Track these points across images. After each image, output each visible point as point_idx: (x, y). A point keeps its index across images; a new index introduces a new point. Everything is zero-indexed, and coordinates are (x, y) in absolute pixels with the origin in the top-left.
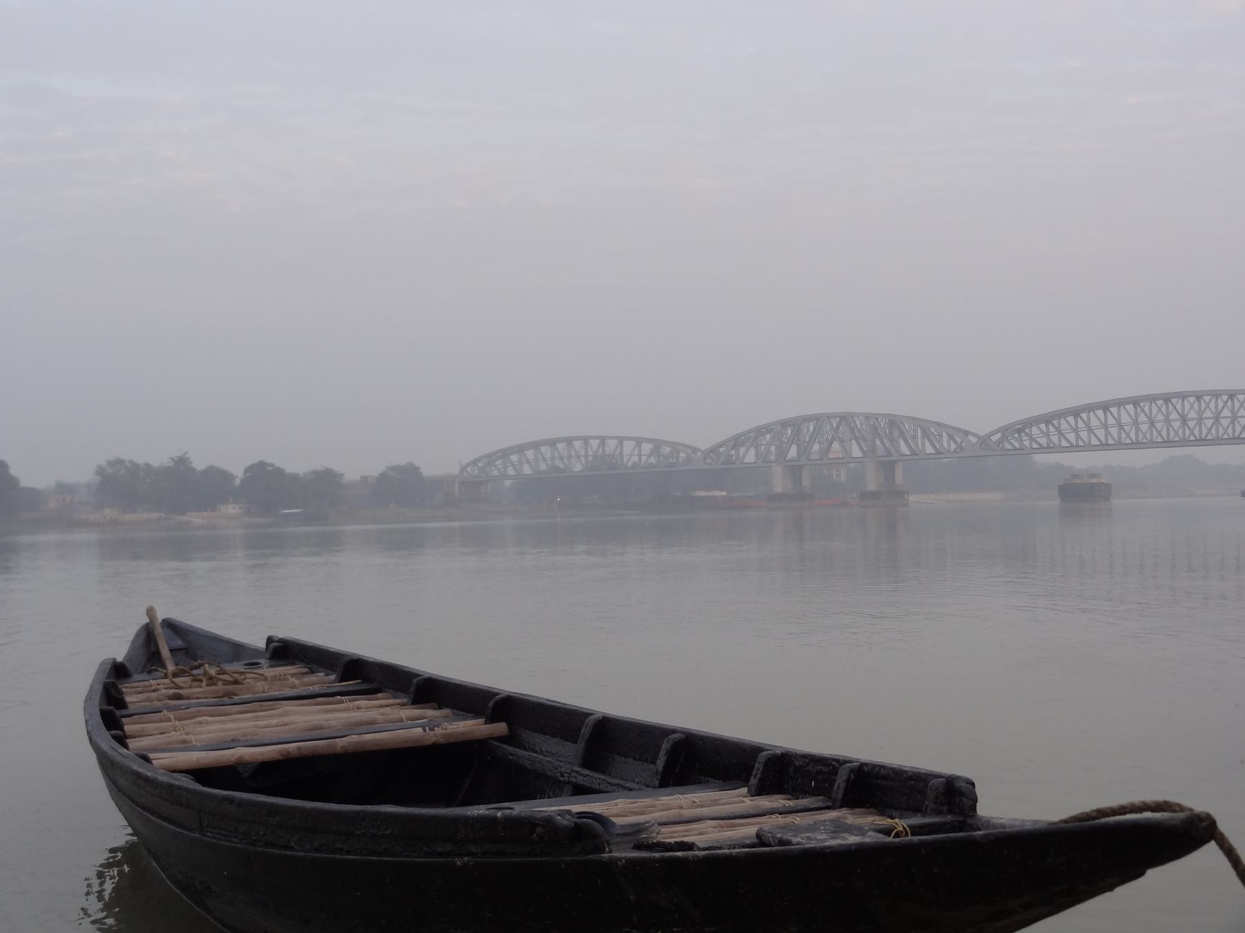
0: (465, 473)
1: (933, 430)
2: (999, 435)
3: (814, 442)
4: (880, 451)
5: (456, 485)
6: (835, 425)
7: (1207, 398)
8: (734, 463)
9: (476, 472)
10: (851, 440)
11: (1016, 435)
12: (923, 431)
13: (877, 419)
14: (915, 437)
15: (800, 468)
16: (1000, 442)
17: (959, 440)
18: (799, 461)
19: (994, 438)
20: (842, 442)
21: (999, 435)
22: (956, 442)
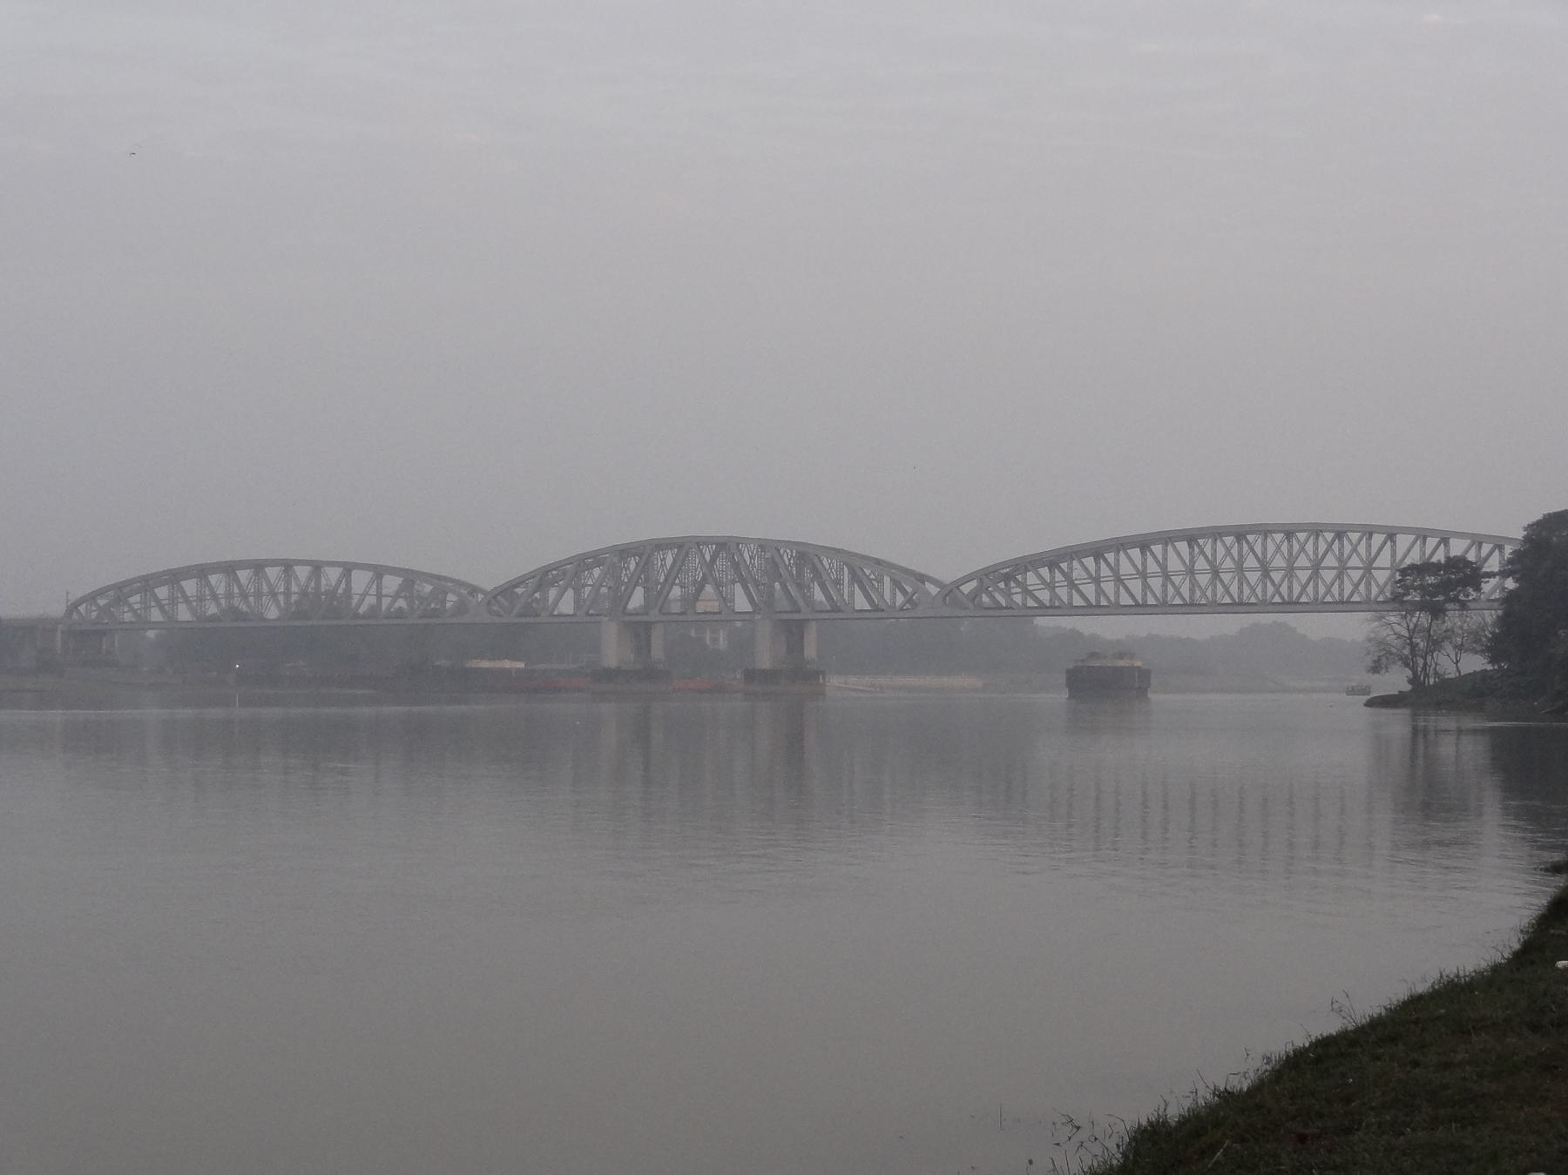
0: (75, 616)
2: (974, 584)
3: (673, 584)
4: (783, 604)
6: (708, 558)
9: (94, 614)
11: (1002, 585)
14: (838, 582)
15: (648, 626)
16: (975, 595)
17: (909, 589)
21: (974, 584)
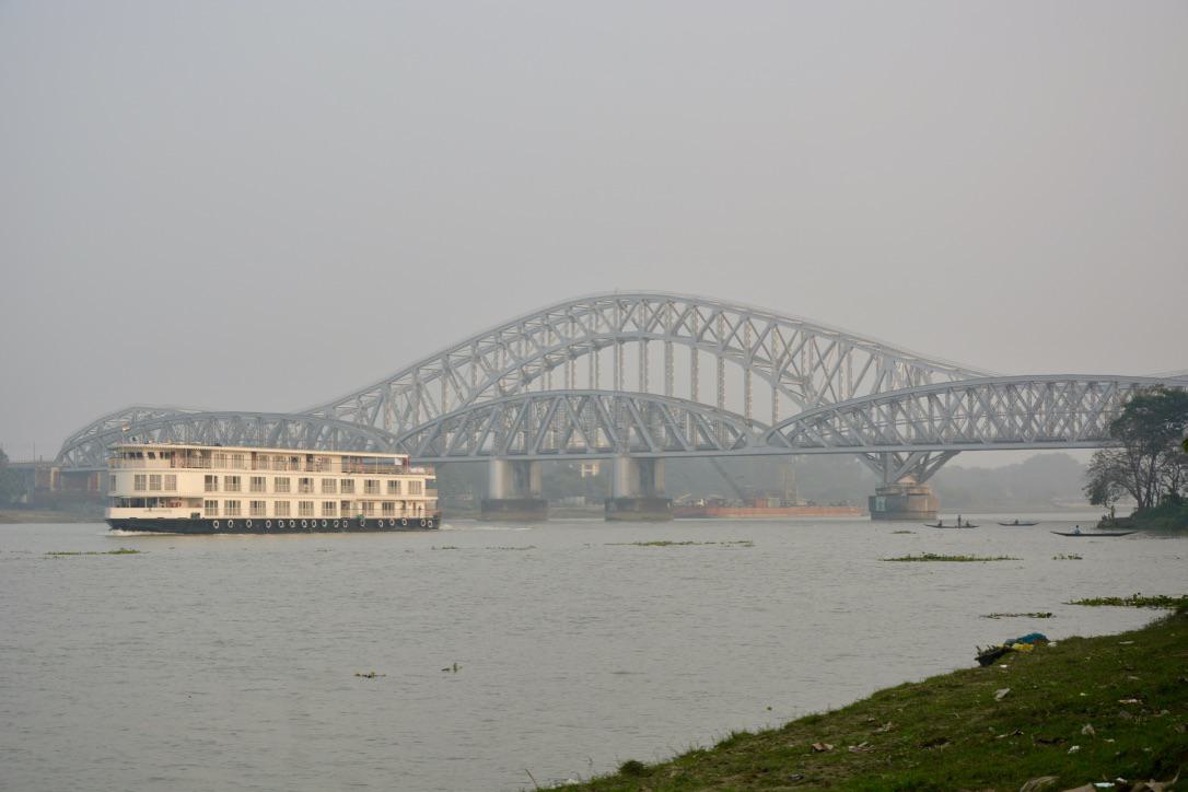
1: (705, 418)
5: (52, 475)
7: (823, 343)
8: (466, 455)
10: (596, 427)
11: (815, 428)
12: (692, 415)
13: (632, 400)
14: (681, 427)
15: (528, 463)
17: (739, 431)
18: (526, 454)
19: (786, 431)
20: (584, 430)
21: (791, 428)
22: (735, 433)
